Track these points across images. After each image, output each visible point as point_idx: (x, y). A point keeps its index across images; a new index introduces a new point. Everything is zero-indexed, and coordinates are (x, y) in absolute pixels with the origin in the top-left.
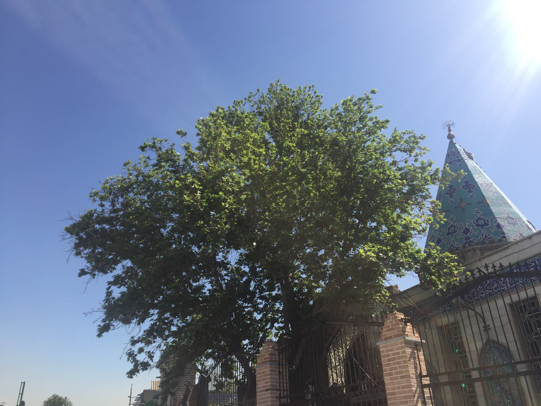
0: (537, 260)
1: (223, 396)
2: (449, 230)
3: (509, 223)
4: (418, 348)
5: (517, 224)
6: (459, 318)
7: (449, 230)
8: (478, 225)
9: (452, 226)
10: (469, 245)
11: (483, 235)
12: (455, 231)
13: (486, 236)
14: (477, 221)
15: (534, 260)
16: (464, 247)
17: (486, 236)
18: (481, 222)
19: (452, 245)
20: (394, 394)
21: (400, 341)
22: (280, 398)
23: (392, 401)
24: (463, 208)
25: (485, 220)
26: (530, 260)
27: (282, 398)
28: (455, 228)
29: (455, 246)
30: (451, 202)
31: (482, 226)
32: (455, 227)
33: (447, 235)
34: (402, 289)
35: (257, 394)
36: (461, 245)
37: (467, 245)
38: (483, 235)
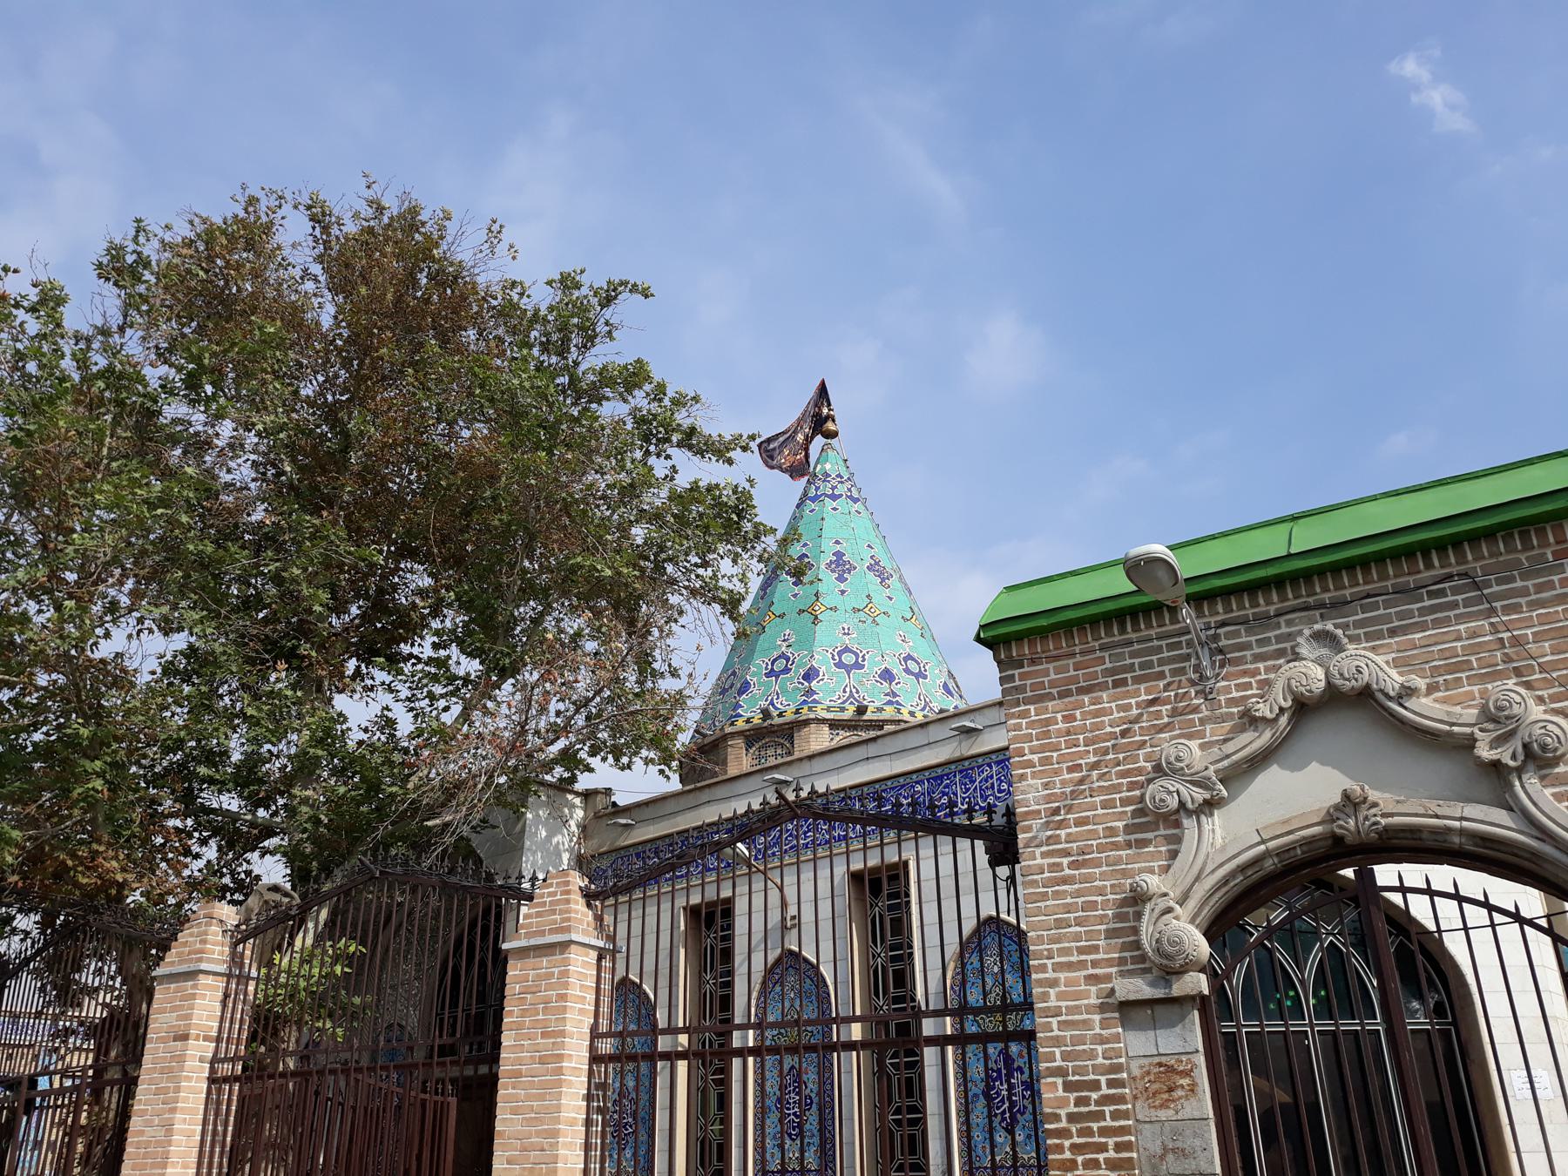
0: (928, 780)
1: (1105, 805)
2: (773, 664)
3: (907, 671)
4: (751, 1032)
5: (925, 677)
6: (908, 854)
7: (773, 664)
8: (840, 665)
9: (783, 656)
10: (810, 709)
11: (844, 691)
12: (786, 670)
13: (851, 695)
14: (906, 659)
15: (921, 777)
16: (797, 712)
17: (851, 695)
18: (848, 659)
19: (772, 703)
20: (518, 1074)
21: (1087, 1109)
22: (215, 1060)
23: (510, 1091)
24: (816, 618)
25: (857, 655)
26: (914, 777)
27: (223, 1061)
28: (788, 661)
29: (779, 706)
30: (795, 596)
31: (848, 669)
32: (788, 659)
33: (767, 675)
34: (622, 800)
35: (147, 1046)
36: (792, 708)
37: (806, 707)
38: (844, 691)
